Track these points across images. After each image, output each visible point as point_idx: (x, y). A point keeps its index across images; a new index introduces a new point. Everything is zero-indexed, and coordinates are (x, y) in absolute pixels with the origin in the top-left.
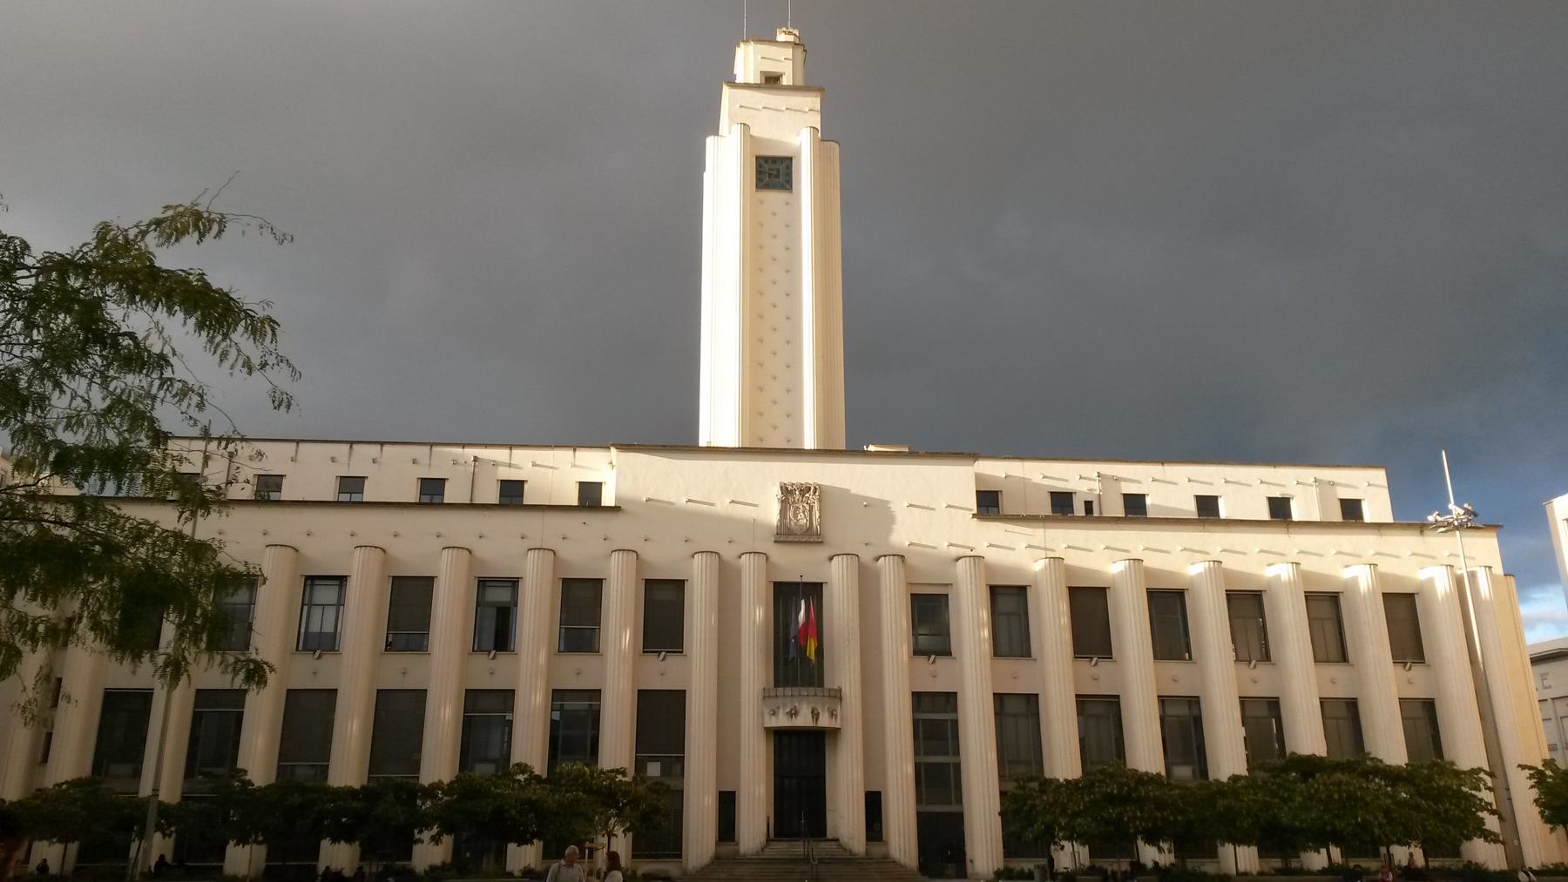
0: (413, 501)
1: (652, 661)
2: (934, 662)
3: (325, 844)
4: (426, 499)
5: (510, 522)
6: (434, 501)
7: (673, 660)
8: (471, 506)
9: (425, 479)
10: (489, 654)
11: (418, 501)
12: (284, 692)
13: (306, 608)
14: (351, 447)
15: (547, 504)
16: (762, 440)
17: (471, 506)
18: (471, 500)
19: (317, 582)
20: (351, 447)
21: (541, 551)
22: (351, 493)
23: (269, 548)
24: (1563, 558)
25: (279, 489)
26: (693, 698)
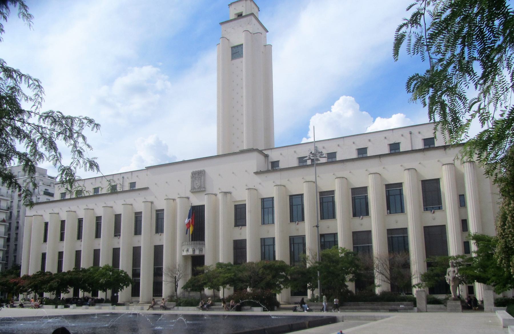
0: (296, 166)
1: (429, 214)
2: (241, 229)
3: (44, 293)
4: (361, 156)
5: (114, 197)
6: (333, 160)
7: (438, 213)
8: (413, 151)
9: (329, 153)
10: (431, 212)
11: (357, 157)
12: (423, 228)
13: (263, 209)
14: (132, 174)
15: (287, 167)
16: (238, 147)
17: (413, 151)
18: (412, 148)
19: (293, 197)
20: (132, 174)
21: (208, 195)
22: (303, 163)
23: (206, 195)
24: (418, 153)
25: (335, 157)
26: (409, 231)
